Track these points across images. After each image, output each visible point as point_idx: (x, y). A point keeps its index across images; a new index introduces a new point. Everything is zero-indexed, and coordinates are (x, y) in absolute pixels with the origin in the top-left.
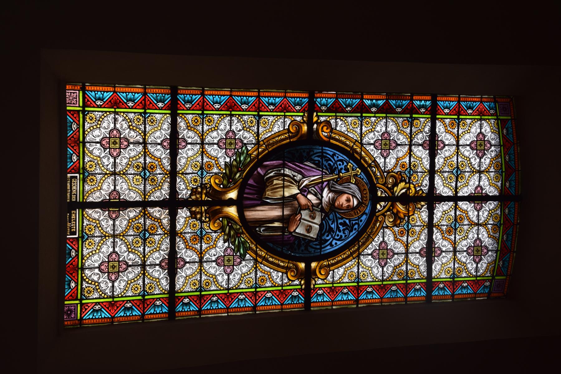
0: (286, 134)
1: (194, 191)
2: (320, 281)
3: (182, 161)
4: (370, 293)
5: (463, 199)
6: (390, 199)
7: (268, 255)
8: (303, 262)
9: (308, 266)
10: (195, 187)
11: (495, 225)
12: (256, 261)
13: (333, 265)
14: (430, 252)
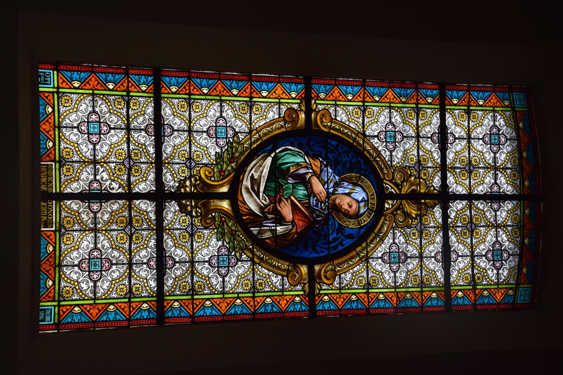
1: (182, 184)
3: (168, 149)
6: (415, 198)
9: (311, 271)
10: (183, 178)
12: (254, 263)
14: (446, 256)
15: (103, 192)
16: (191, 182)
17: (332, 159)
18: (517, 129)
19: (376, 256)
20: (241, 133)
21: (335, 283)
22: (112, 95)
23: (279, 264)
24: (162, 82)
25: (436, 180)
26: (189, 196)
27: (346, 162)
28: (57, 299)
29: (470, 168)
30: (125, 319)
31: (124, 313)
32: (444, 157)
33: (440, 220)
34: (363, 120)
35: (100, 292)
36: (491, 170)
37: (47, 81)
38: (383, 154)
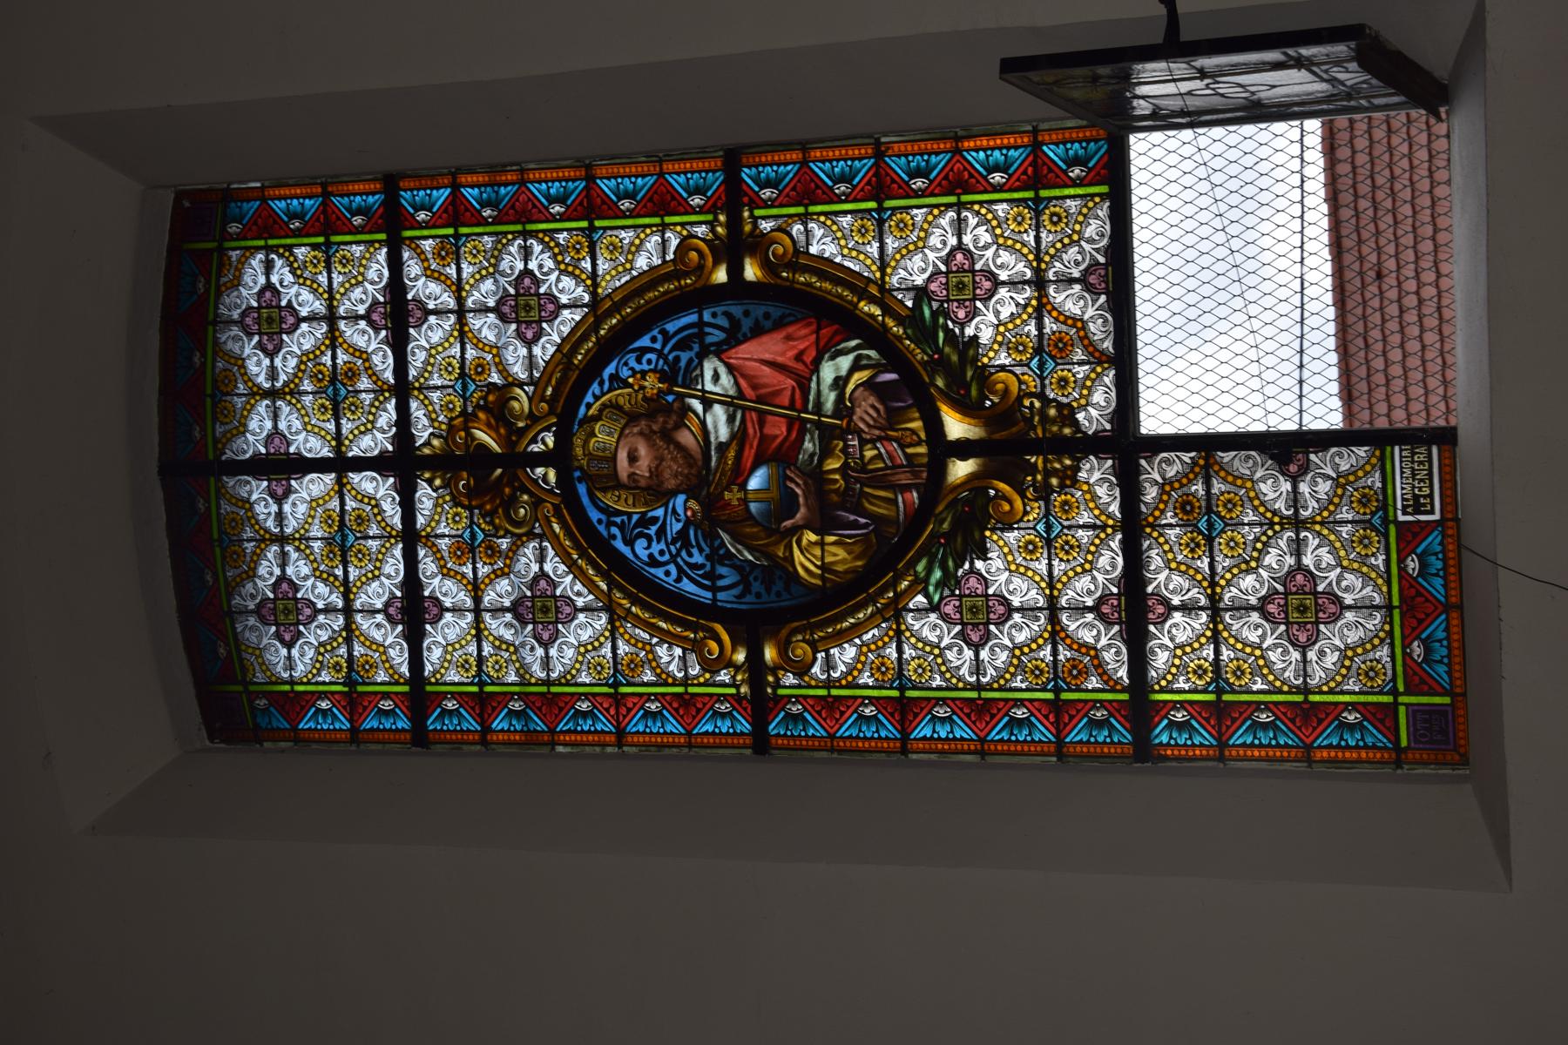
0: (822, 638)
1: (1070, 479)
2: (701, 230)
3: (1111, 560)
4: (996, 168)
5: (320, 465)
6: (488, 469)
7: (851, 303)
8: (751, 283)
9: (736, 271)
11: (228, 394)
13: (667, 277)
14: (398, 315)
18: (237, 642)
25: (428, 504)
32: (411, 561)
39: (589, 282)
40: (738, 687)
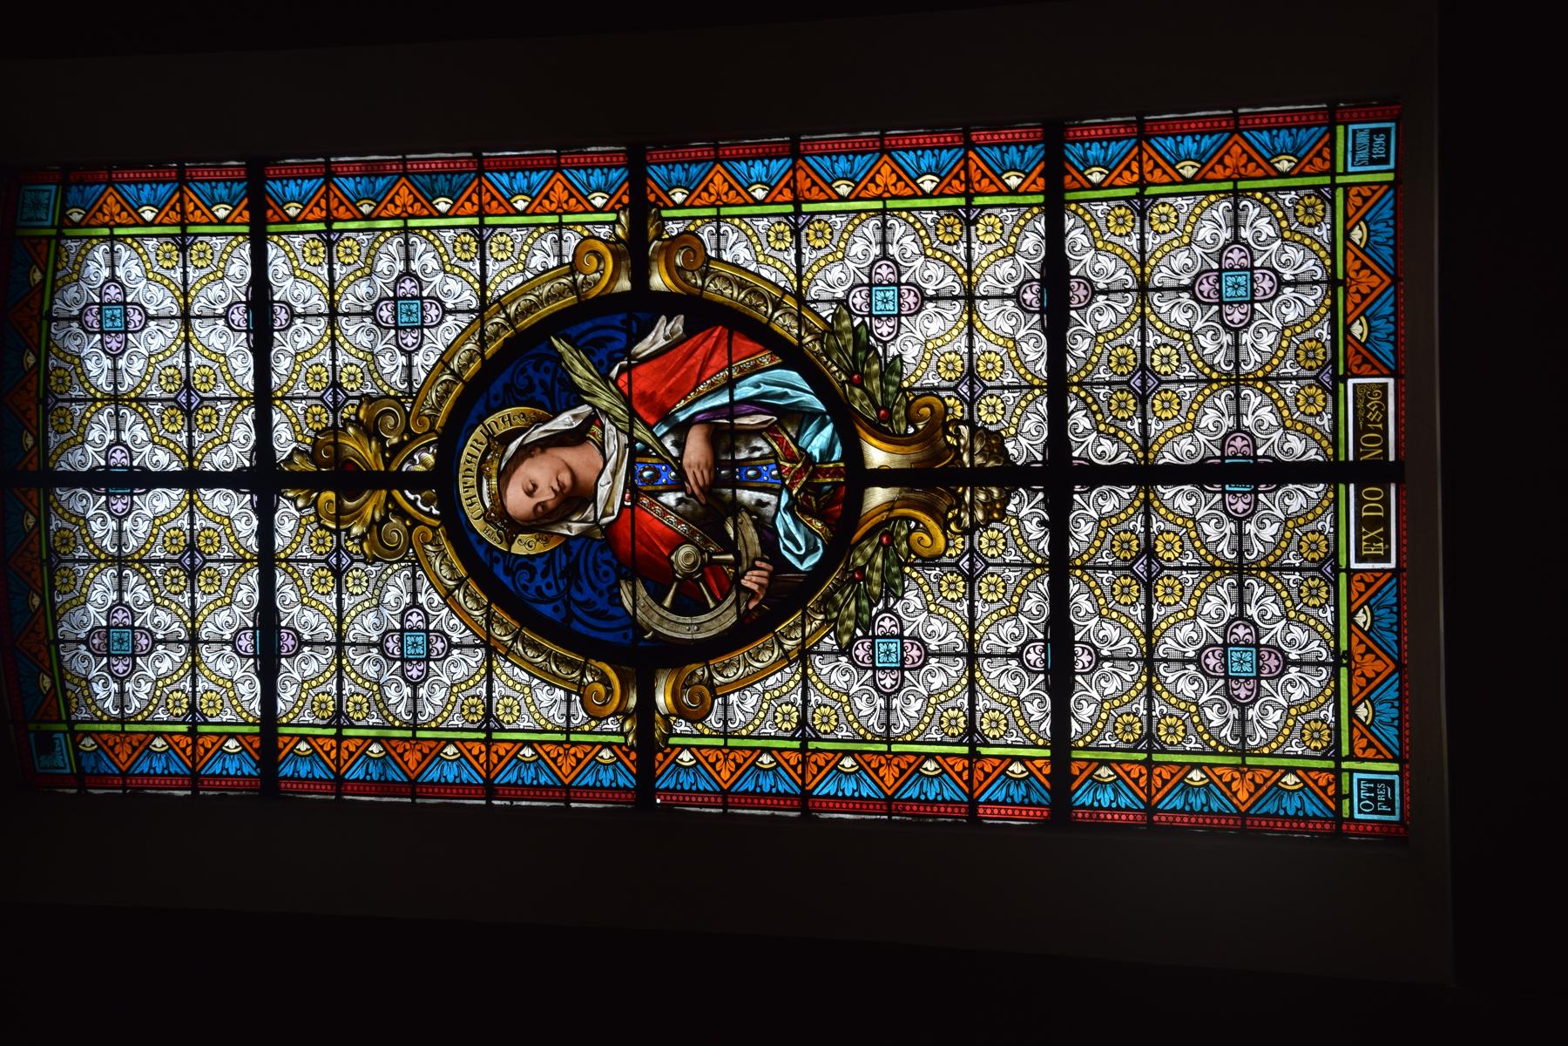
1: (995, 511)
5: (165, 480)
6: (358, 474)
8: (659, 293)
9: (640, 277)
10: (993, 525)
12: (799, 296)
15: (1218, 487)
16: (972, 515)
17: (585, 585)
18: (61, 673)
19: (459, 316)
20: (832, 652)
21: (574, 244)
22: (842, 741)
23: (728, 292)
24: (1048, 785)
26: (978, 477)
27: (544, 575)
28: (1340, 192)
29: (191, 560)
30: (809, 159)
31: (1153, 154)
32: (267, 588)
33: (276, 418)
34: (340, 687)
35: (871, 228)
36: (1257, 562)
37: (1369, 790)
38: (437, 598)
39: (477, 286)
40: (626, 735)
